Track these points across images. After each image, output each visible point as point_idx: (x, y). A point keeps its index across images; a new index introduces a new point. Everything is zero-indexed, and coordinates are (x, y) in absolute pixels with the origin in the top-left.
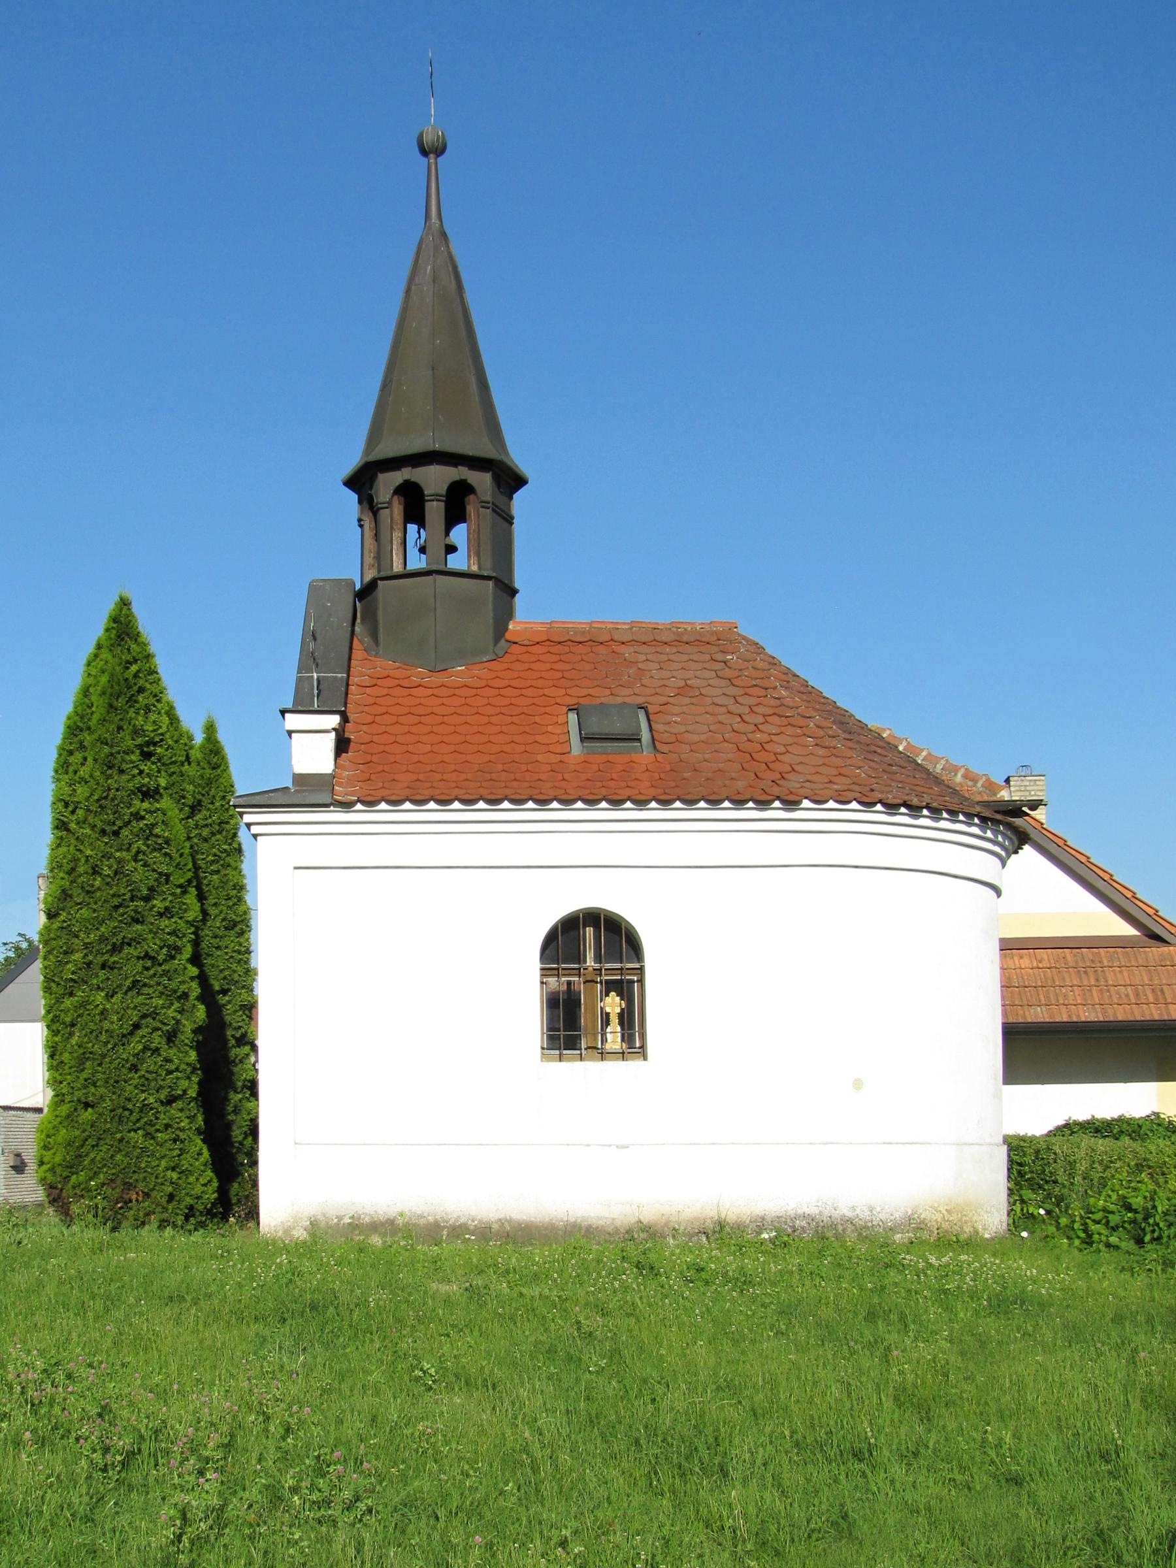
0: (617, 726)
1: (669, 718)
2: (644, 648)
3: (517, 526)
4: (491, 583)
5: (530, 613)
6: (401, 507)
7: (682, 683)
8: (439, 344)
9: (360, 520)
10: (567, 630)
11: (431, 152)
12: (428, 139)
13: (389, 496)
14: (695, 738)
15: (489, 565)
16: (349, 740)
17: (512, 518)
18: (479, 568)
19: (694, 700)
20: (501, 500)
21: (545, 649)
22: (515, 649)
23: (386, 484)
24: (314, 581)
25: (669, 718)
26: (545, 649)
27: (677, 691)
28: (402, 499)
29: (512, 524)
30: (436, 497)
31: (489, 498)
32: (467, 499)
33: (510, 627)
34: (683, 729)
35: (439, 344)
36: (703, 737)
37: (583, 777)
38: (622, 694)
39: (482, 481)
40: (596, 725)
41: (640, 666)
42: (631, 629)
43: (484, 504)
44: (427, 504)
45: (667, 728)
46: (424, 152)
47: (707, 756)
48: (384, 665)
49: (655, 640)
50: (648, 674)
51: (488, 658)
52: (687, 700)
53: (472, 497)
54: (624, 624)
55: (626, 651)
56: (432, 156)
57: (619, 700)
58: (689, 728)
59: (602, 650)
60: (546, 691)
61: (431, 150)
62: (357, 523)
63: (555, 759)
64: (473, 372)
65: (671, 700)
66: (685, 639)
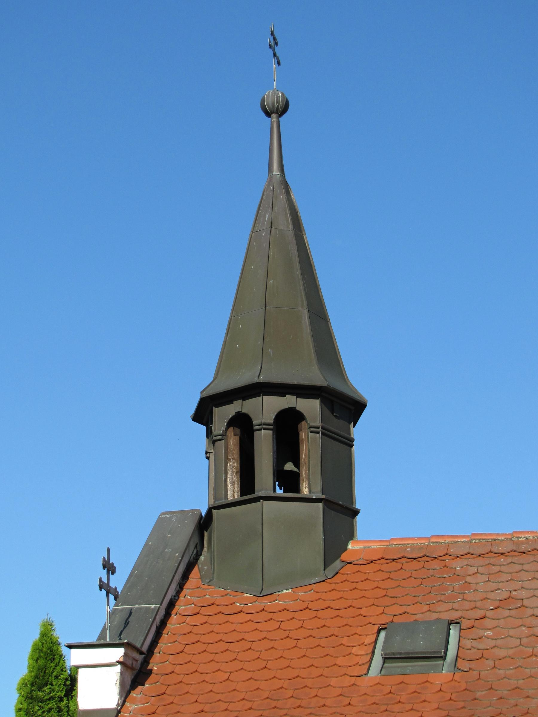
0: (420, 645)
1: (481, 633)
2: (480, 561)
3: (355, 449)
4: (321, 505)
5: (371, 530)
6: (237, 438)
7: (505, 595)
8: (286, 281)
9: (207, 453)
10: (405, 546)
11: (273, 112)
12: (269, 103)
13: (223, 428)
14: (502, 653)
15: (319, 488)
16: (150, 672)
17: (353, 440)
18: (310, 492)
19: (513, 612)
20: (335, 425)
21: (377, 567)
22: (349, 568)
23: (223, 414)
24: (163, 513)
25: (481, 633)
26: (377, 567)
27: (497, 604)
28: (238, 431)
29: (352, 446)
30: (264, 426)
31: (318, 423)
32: (299, 426)
33: (350, 547)
34: (493, 643)
35: (286, 281)
36: (511, 652)
37: (371, 700)
38: (439, 609)
39: (310, 407)
40: (401, 645)
41: (468, 579)
42: (470, 542)
43: (313, 429)
44: (256, 434)
45: (475, 644)
46: (268, 114)
47: (508, 672)
48: (214, 593)
49: (490, 552)
50: (474, 587)
51: (317, 579)
52: (507, 613)
53: (303, 422)
54: (464, 536)
55: (458, 565)
56: (274, 116)
57: (434, 616)
58: (499, 642)
59: (435, 565)
60: (363, 612)
61: (278, 110)
62: (205, 456)
63: (347, 681)
64: (306, 306)
65: (489, 614)
66: (523, 548)
